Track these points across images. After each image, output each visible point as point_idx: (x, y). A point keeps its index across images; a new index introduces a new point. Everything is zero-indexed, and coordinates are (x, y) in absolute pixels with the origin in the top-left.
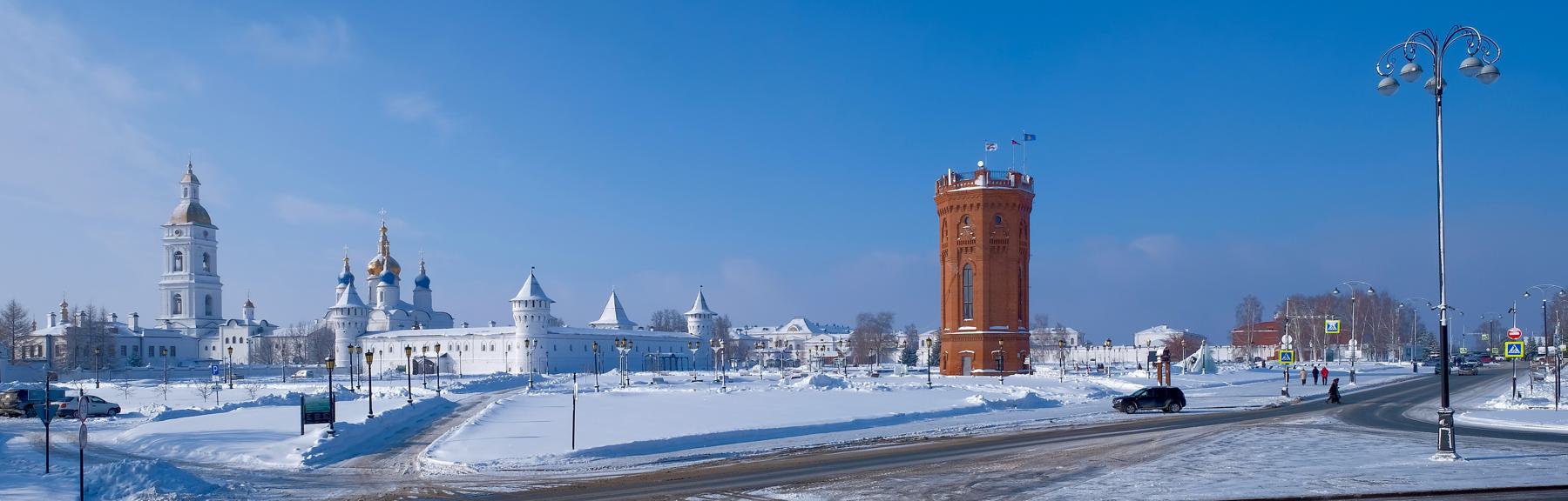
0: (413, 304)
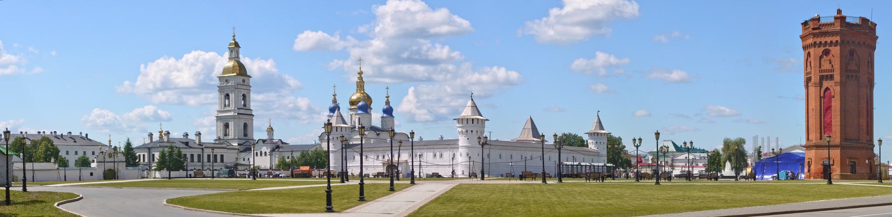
0: (381, 127)
